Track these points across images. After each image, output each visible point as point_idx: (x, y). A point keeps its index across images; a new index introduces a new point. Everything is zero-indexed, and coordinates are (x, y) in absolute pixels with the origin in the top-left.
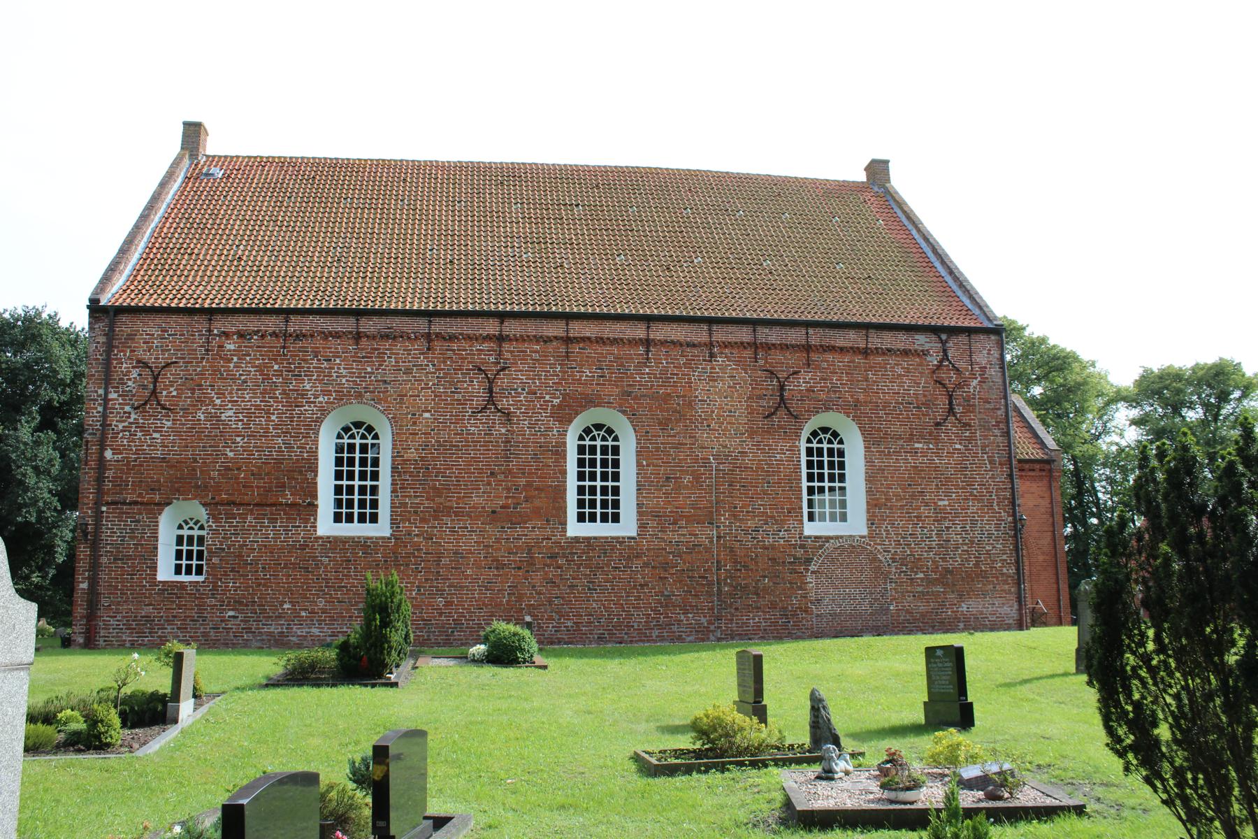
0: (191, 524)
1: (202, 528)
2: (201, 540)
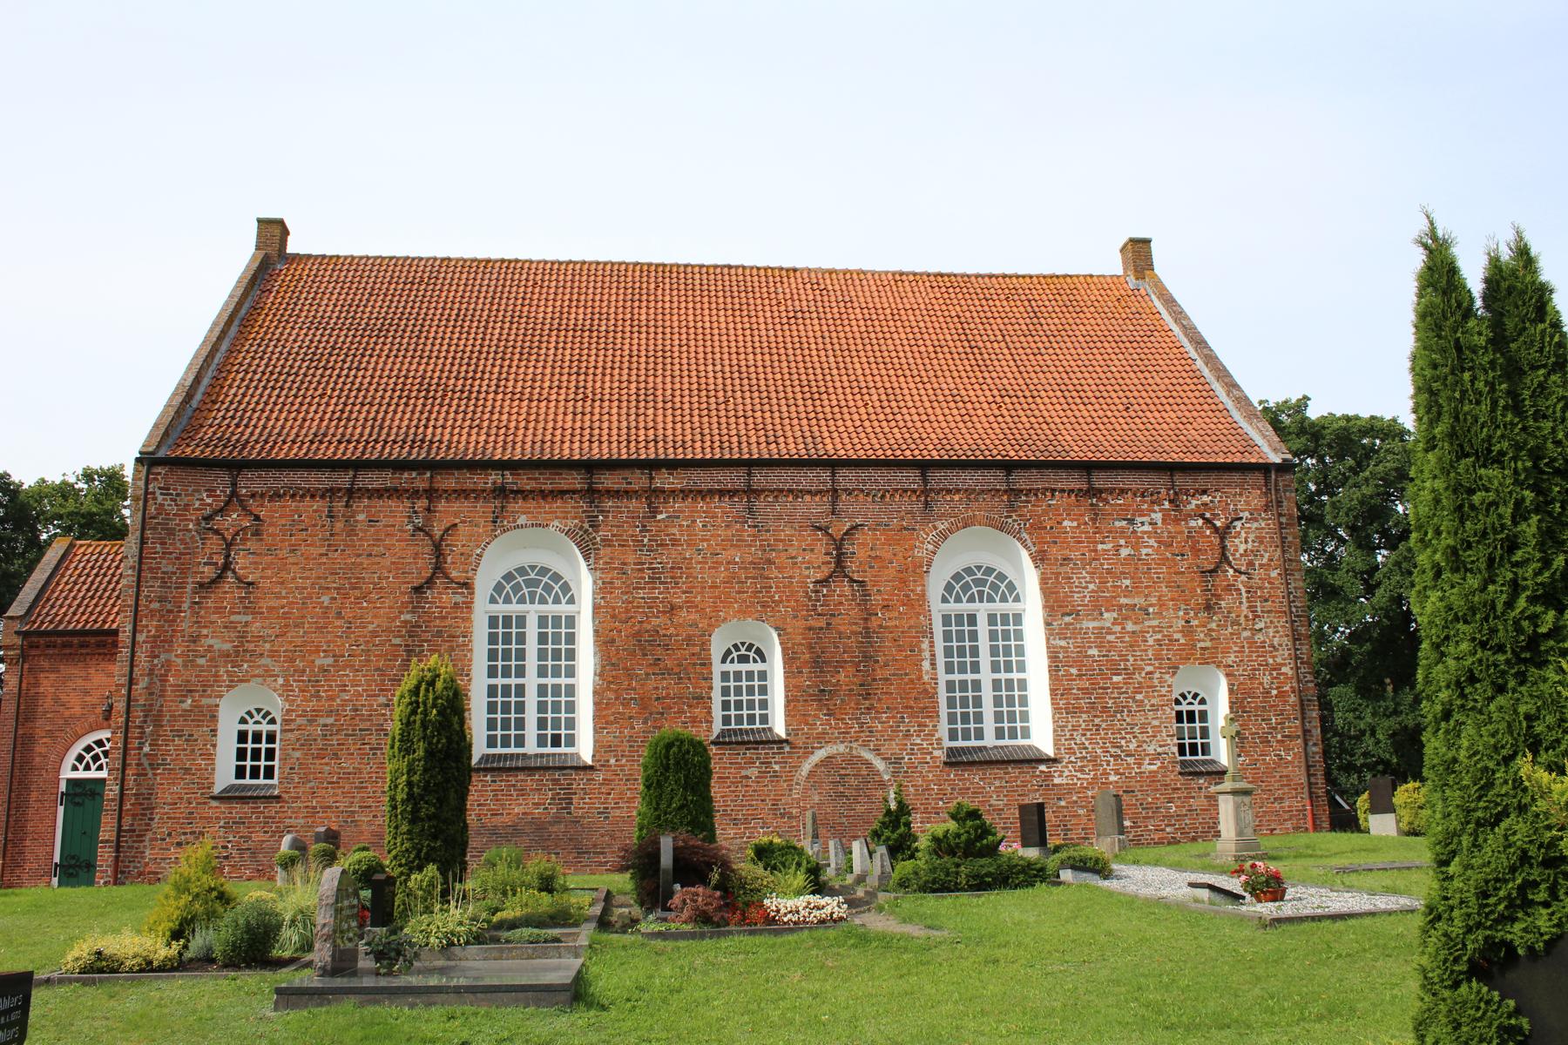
0: (1190, 699)
1: (273, 721)
2: (271, 738)
